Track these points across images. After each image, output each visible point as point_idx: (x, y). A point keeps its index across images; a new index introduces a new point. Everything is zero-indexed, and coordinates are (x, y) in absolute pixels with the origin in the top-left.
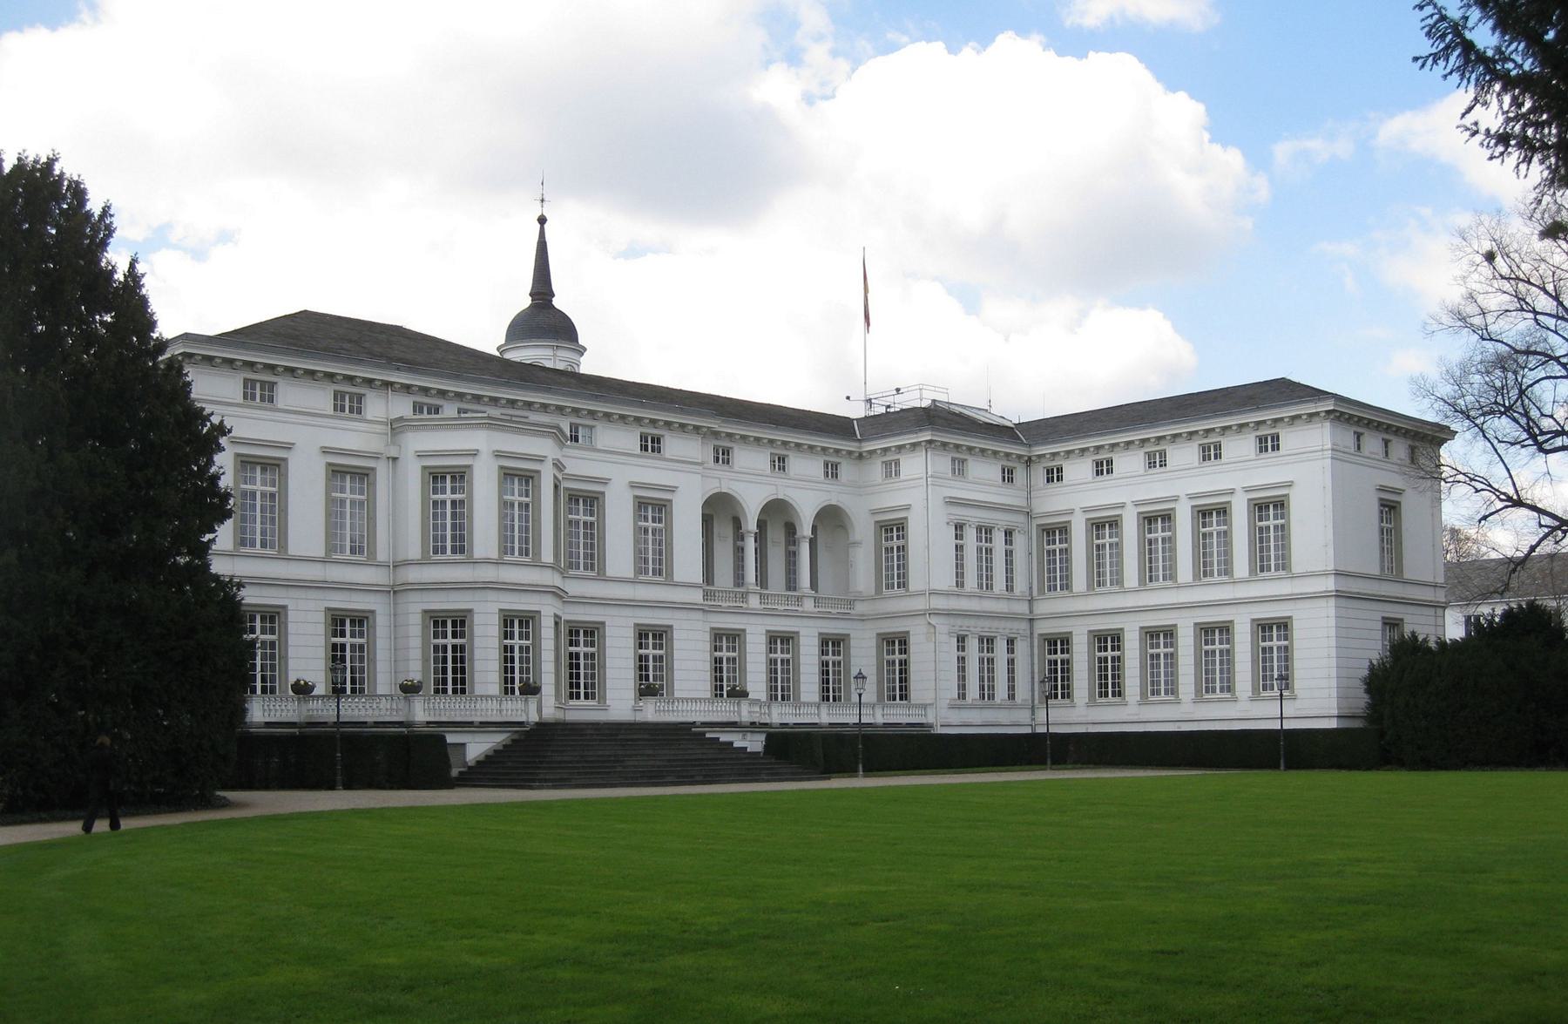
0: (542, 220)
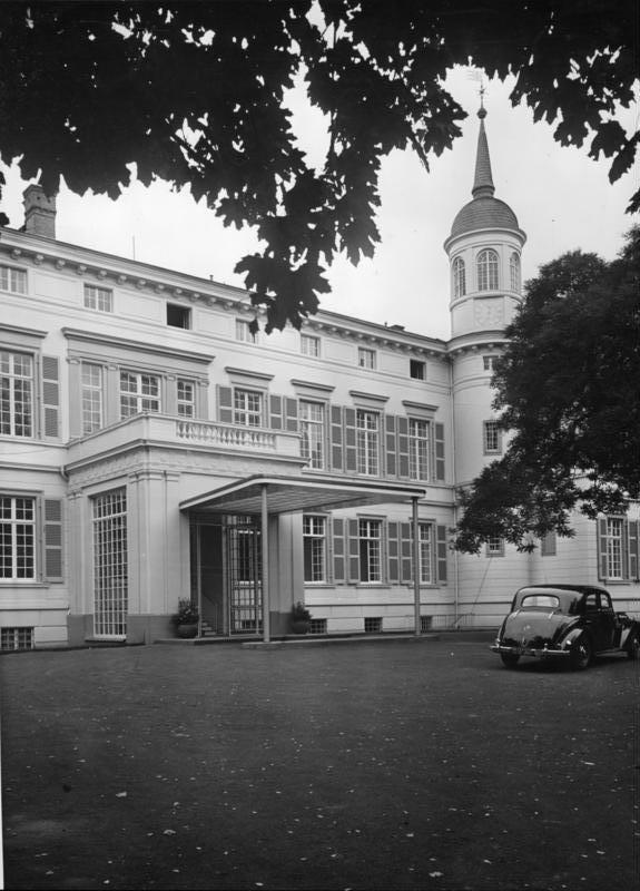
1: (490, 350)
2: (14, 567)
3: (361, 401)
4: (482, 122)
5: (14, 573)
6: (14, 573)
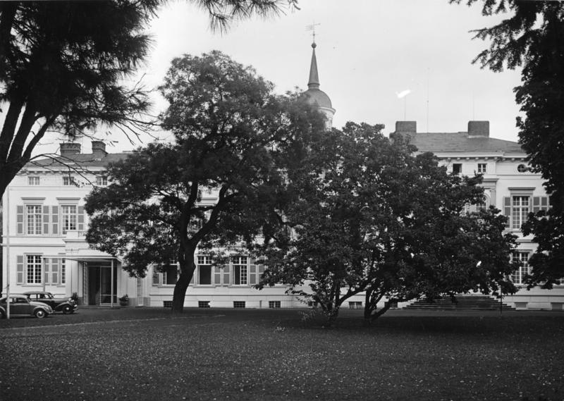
0: (314, 46)
1: (458, 161)
2: (34, 279)
3: (61, 202)
4: (314, 51)
5: (34, 281)
6: (34, 281)
